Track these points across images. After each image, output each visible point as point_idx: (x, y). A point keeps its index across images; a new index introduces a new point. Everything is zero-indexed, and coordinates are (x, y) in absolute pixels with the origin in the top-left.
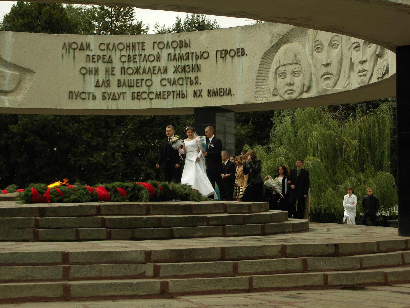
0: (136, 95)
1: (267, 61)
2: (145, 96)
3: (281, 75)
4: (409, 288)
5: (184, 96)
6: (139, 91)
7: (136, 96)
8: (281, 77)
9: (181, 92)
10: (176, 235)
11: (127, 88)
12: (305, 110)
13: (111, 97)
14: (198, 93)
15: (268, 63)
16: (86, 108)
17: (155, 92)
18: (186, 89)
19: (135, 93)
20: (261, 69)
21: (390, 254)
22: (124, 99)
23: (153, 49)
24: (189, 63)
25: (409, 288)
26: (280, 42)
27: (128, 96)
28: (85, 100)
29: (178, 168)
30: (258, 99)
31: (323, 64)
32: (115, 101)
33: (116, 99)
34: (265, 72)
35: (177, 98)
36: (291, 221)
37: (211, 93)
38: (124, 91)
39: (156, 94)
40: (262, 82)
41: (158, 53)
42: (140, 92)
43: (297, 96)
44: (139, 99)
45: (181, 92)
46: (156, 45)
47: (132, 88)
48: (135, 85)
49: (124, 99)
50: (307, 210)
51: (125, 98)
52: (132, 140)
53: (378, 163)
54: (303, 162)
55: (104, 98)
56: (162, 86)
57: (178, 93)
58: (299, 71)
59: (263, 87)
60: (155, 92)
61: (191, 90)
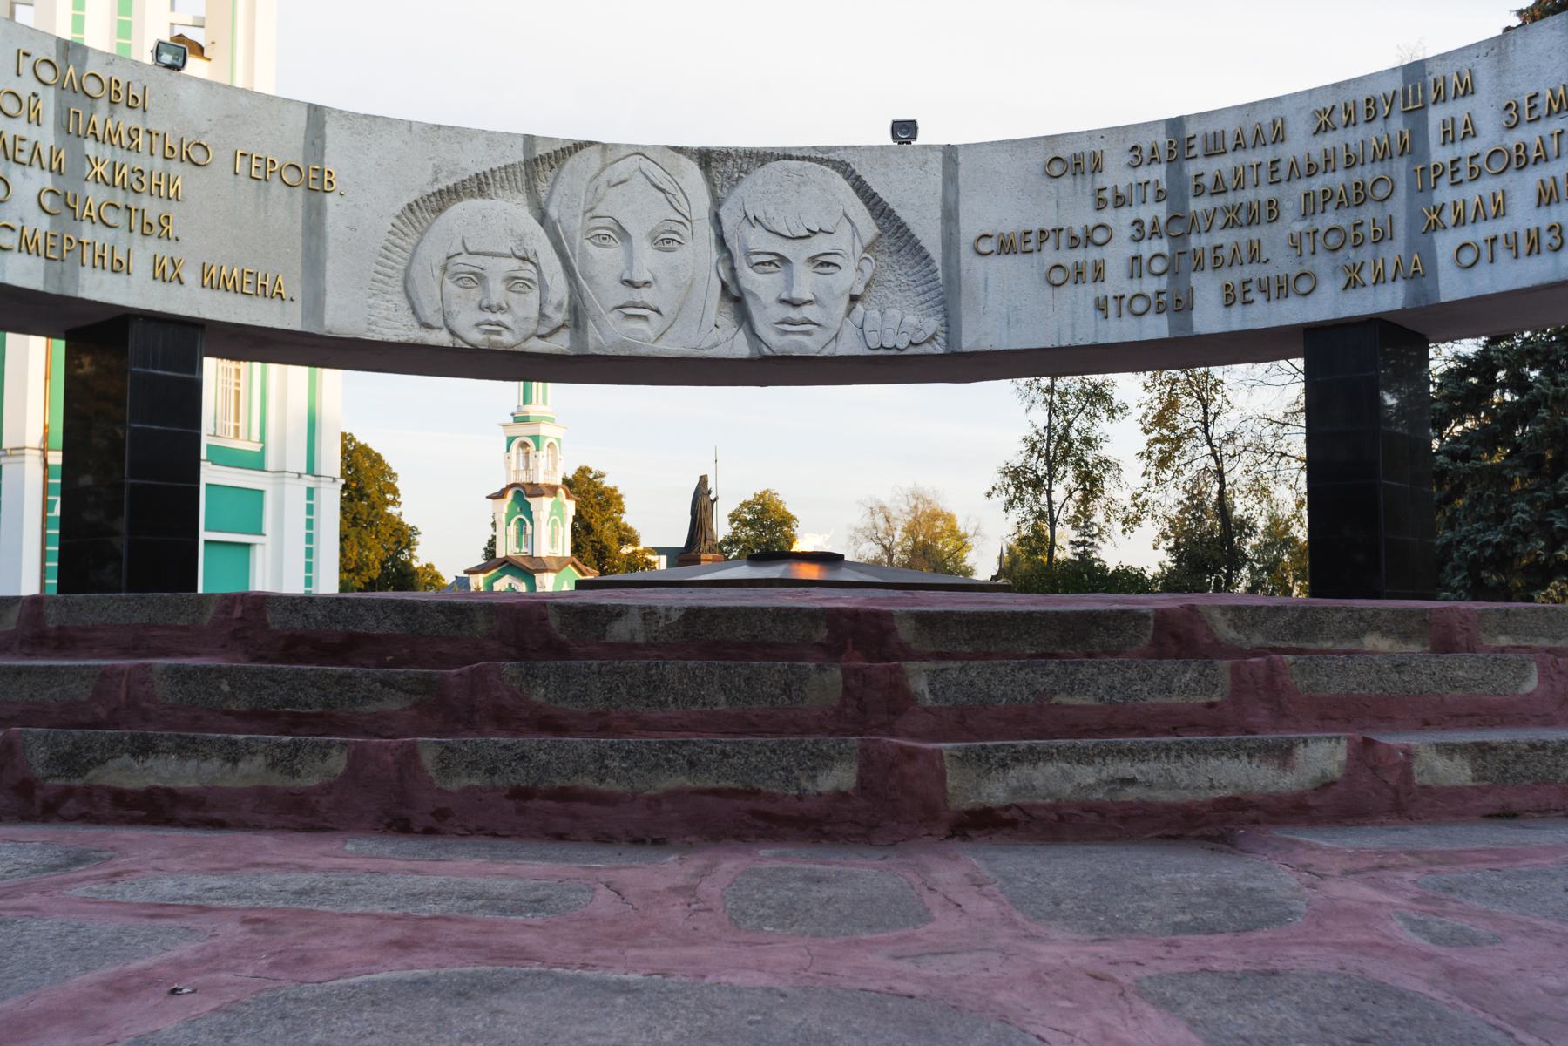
1: (405, 230)
3: (462, 275)
5: (120, 267)
8: (460, 283)
15: (406, 235)
18: (126, 247)
20: (390, 246)
21: (359, 599)
23: (18, 75)
24: (1247, 195)
26: (460, 188)
30: (374, 327)
34: (395, 257)
36: (1311, 848)
37: (214, 281)
40: (386, 284)
41: (35, 95)
46: (26, 65)
54: (1249, 639)
56: (1048, 286)
58: (529, 280)
59: (388, 297)
61: (143, 253)
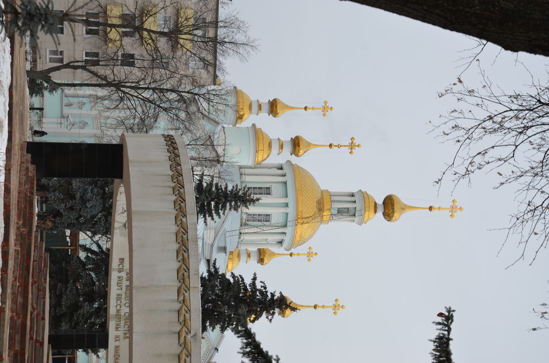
4: (548, 130)
5: (117, 329)
7: (119, 297)
9: (120, 326)
11: (116, 314)
13: (119, 281)
14: (117, 339)
17: (121, 309)
19: (121, 296)
25: (548, 130)
27: (119, 292)
31: (232, 271)
33: (117, 284)
38: (123, 289)
39: (119, 310)
43: (236, 100)
44: (117, 299)
45: (120, 326)
47: (124, 294)
48: (126, 296)
52: (71, 350)
53: (93, 320)
57: (119, 325)
60: (121, 309)
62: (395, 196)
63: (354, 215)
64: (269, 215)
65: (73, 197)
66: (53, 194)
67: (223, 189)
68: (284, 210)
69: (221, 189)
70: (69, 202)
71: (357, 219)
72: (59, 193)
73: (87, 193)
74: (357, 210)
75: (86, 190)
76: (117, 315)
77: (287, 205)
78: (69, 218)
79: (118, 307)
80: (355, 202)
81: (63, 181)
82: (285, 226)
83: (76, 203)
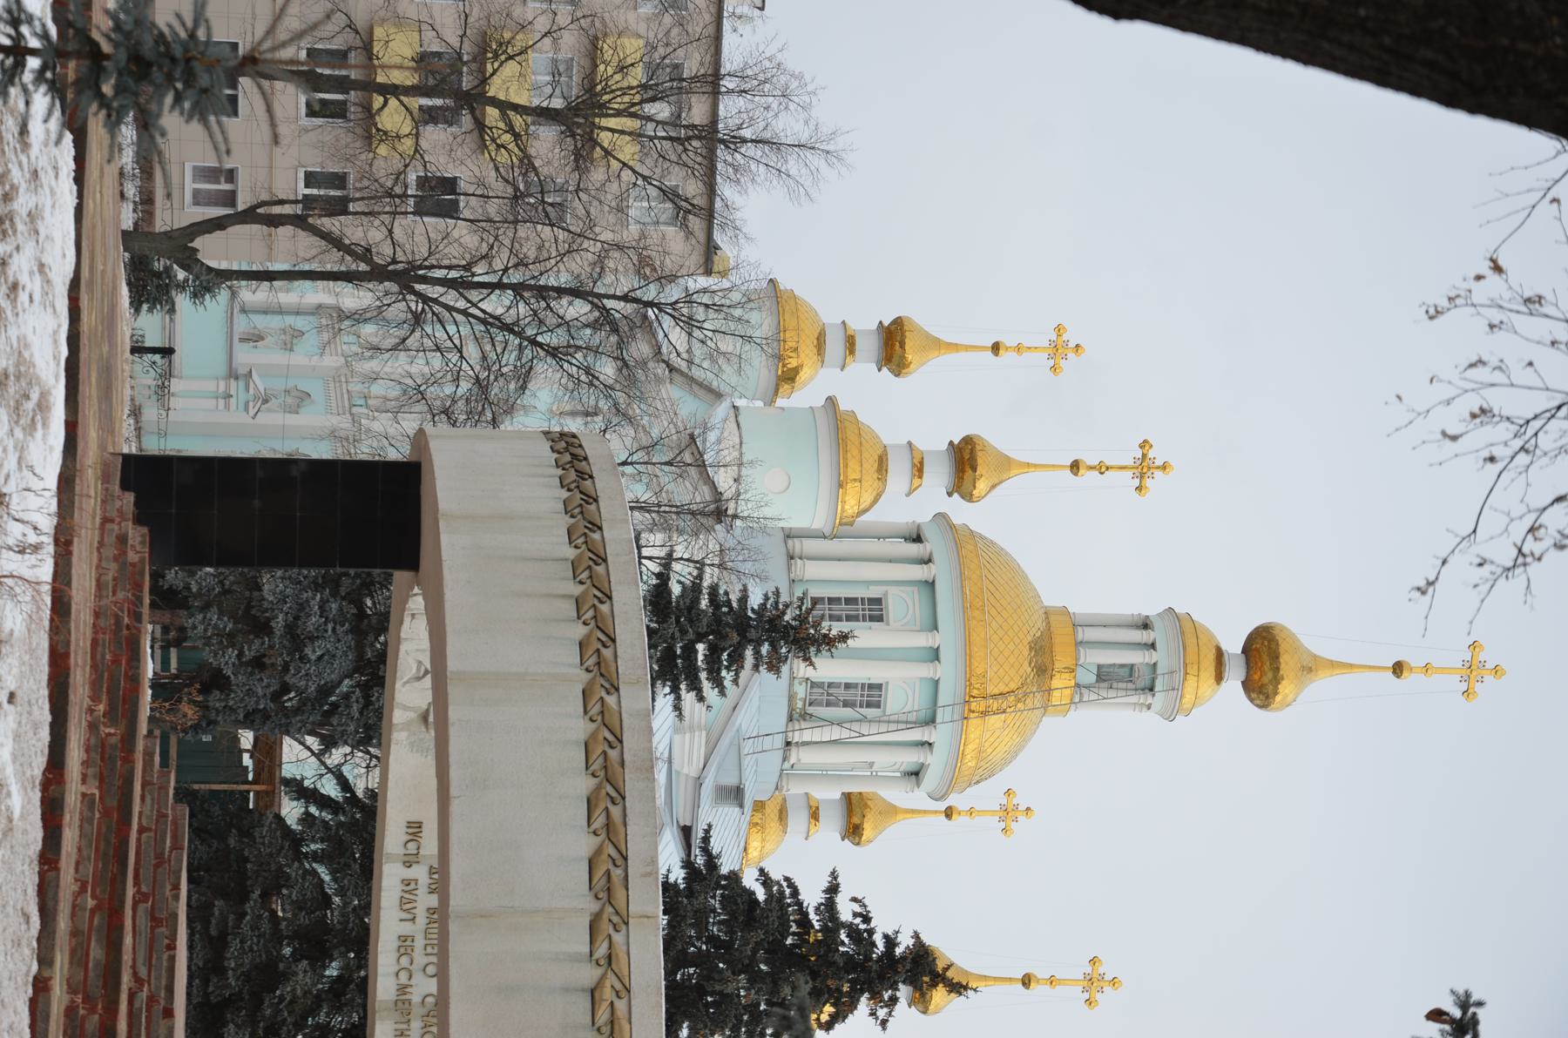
0: (408, 943)
2: (405, 961)
6: (415, 949)
10: (227, 47)
12: (434, 136)
13: (407, 896)
16: (441, 530)
19: (413, 941)
22: (401, 920)
27: (407, 928)
28: (395, 978)
29: (700, 642)
32: (398, 903)
35: (396, 1030)
39: (406, 986)
42: (412, 950)
44: (399, 951)
47: (423, 935)
48: (428, 942)
49: (401, 920)
50: (195, 702)
51: (403, 923)
53: (322, 1018)
55: (407, 882)
60: (412, 982)
62: (1283, 628)
63: (1151, 689)
64: (879, 687)
65: (262, 627)
66: (200, 617)
67: (735, 605)
68: (925, 671)
69: (729, 602)
70: (250, 643)
71: (1158, 700)
72: (221, 614)
73: (309, 616)
74: (1159, 671)
75: (302, 606)
76: (400, 1004)
77: (935, 655)
78: (250, 692)
79: (403, 976)
80: (1153, 646)
81: (232, 578)
82: (931, 721)
83: (271, 647)
